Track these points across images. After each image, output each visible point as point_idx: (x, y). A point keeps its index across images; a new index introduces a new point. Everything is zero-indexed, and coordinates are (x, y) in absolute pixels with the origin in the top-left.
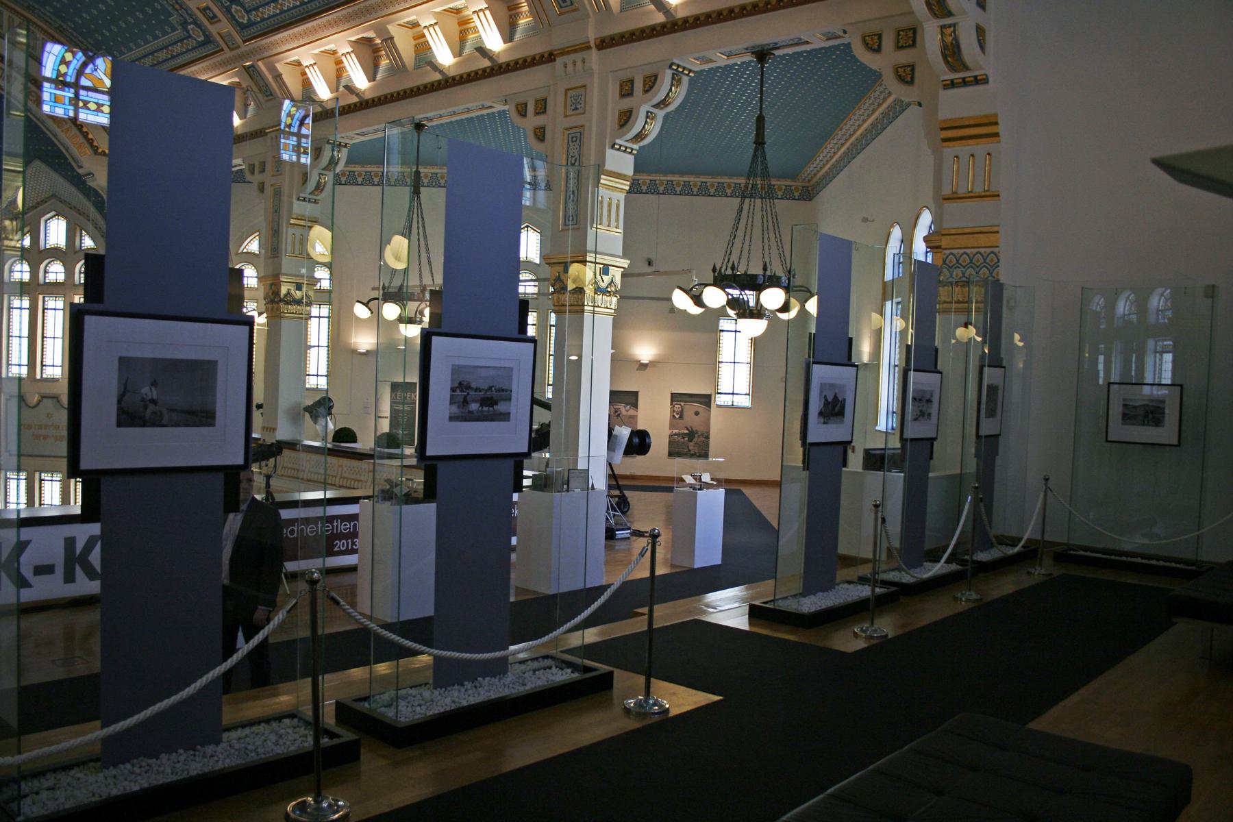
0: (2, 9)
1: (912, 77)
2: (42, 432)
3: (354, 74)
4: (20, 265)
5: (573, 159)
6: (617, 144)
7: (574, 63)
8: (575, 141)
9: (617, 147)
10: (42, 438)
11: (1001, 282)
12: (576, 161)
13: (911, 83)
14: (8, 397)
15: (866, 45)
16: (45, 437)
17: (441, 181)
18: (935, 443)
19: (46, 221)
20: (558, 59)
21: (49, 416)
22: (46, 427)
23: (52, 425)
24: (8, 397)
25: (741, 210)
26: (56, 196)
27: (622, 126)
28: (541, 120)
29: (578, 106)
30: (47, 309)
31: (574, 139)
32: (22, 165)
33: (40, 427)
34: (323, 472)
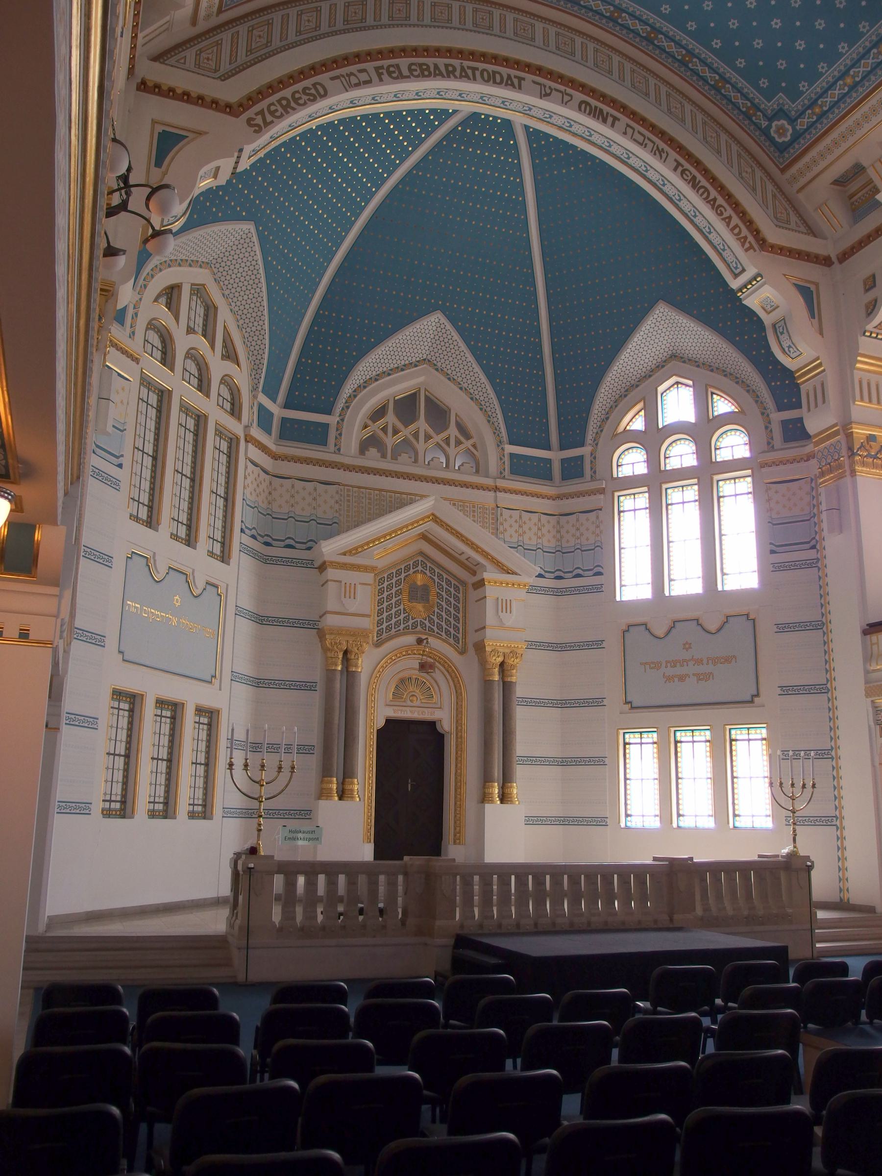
2: (679, 670)
4: (743, 443)
5: (781, 328)
6: (868, 331)
9: (868, 334)
10: (676, 679)
11: (367, 452)
12: (783, 329)
14: (751, 617)
16: (682, 678)
18: (813, 873)
19: (677, 383)
21: (687, 646)
22: (683, 662)
23: (692, 659)
24: (751, 617)
26: (676, 356)
27: (869, 314)
30: (623, 511)
33: (674, 664)
34: (196, 803)
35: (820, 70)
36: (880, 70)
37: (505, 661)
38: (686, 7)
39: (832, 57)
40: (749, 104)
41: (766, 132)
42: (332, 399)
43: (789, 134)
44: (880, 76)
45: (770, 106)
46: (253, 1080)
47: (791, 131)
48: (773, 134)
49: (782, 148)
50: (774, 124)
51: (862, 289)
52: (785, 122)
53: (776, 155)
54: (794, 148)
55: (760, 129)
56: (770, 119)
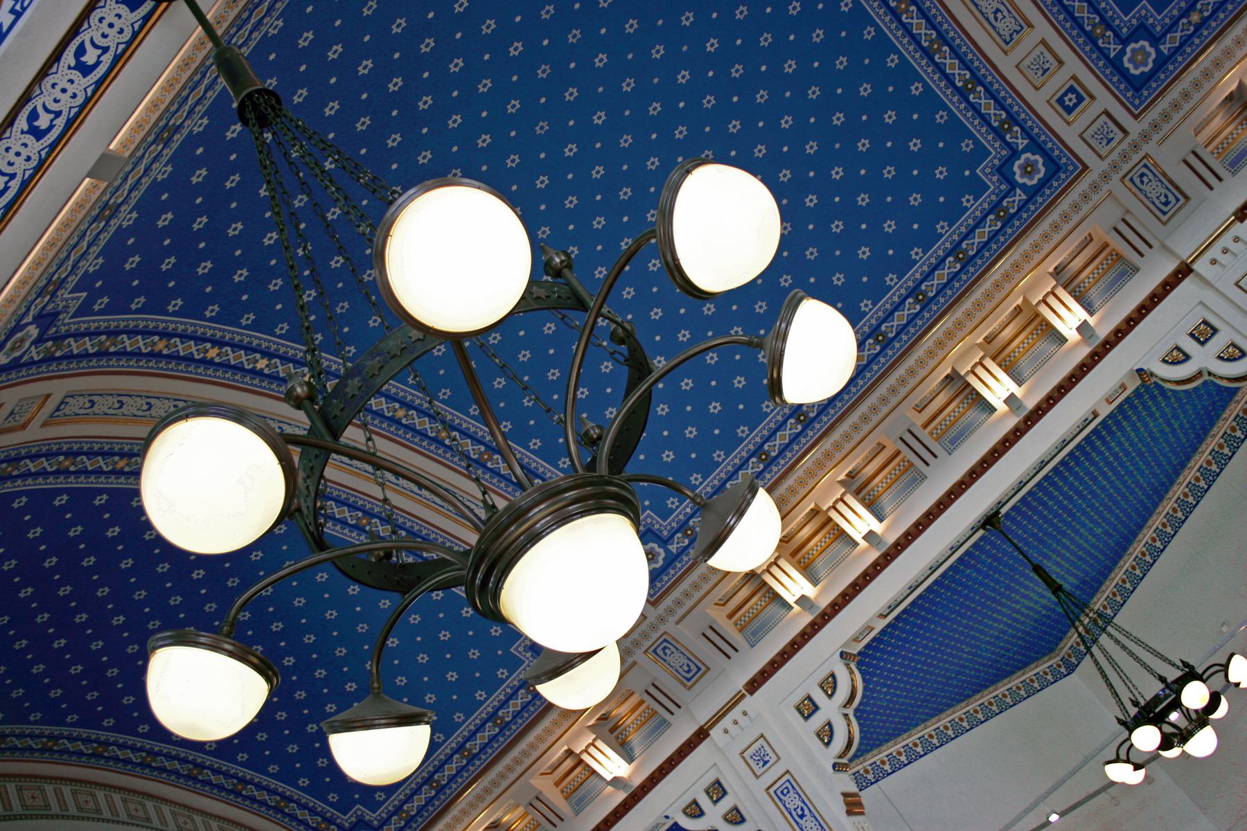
0: (241, 4)
1: (741, 816)
3: (1059, 316)
7: (736, 723)
8: (788, 792)
13: (743, 820)
15: (834, 688)
17: (869, 777)
20: (711, 732)
25: (1096, 663)
28: (726, 804)
29: (767, 758)
31: (785, 792)
32: (271, 88)
35: (965, 204)
36: (924, 3)
37: (1035, 563)
38: (838, 253)
39: (906, 73)
40: (992, 217)
41: (1033, 193)
42: (561, 440)
43: (1032, 158)
44: (932, 2)
45: (993, 184)
46: (532, 484)
47: (1028, 155)
48: (1035, 182)
49: (1054, 168)
50: (1021, 181)
51: (1162, 354)
52: (1017, 163)
53: (1063, 176)
54: (1052, 150)
55: (1027, 202)
56: (1013, 185)
